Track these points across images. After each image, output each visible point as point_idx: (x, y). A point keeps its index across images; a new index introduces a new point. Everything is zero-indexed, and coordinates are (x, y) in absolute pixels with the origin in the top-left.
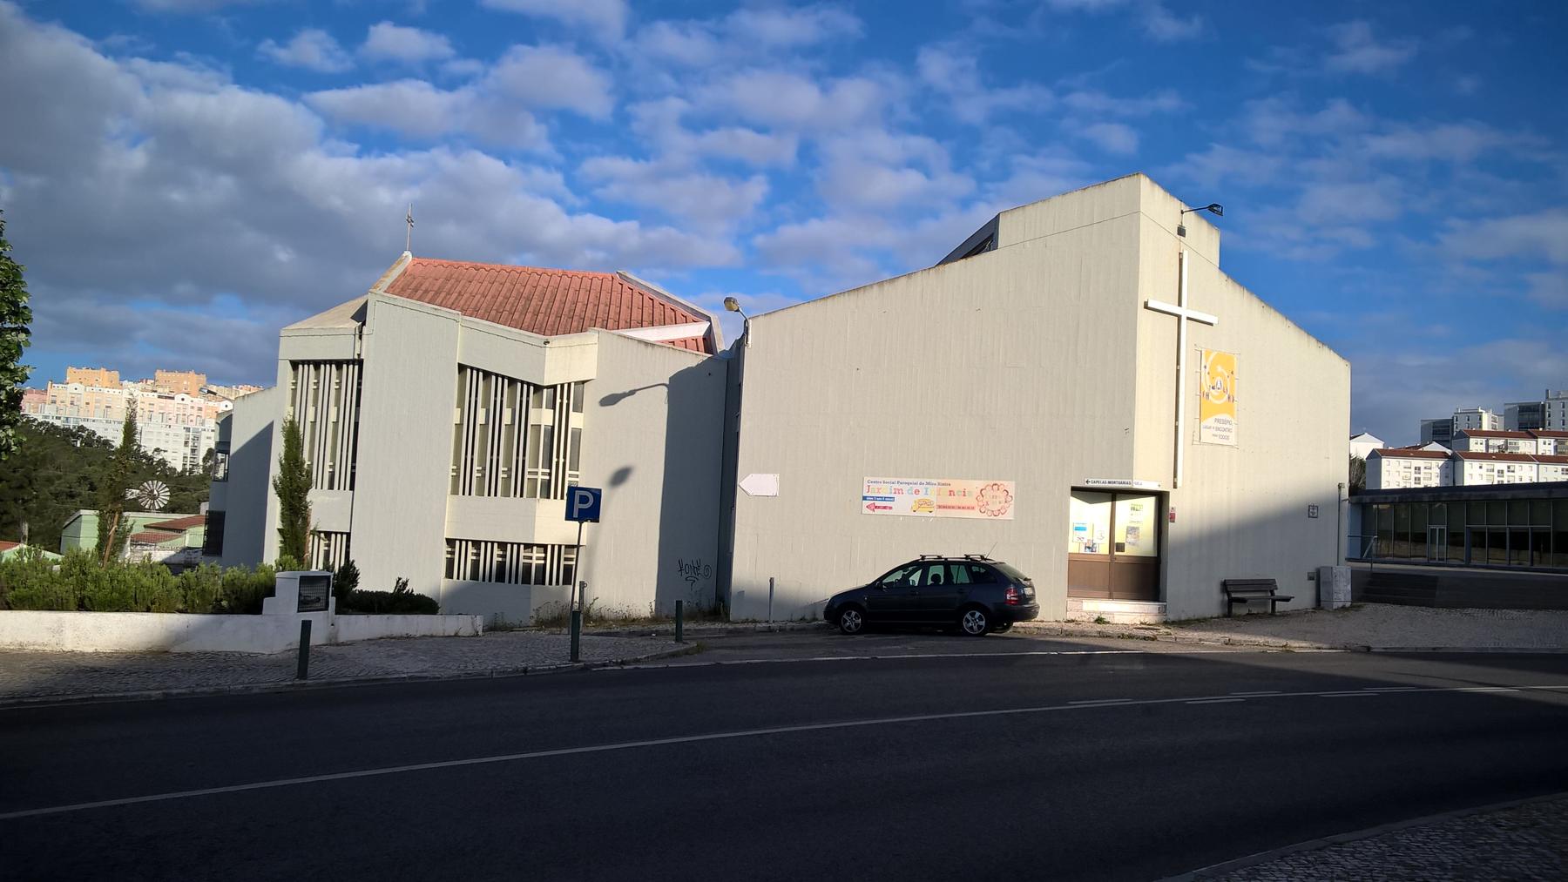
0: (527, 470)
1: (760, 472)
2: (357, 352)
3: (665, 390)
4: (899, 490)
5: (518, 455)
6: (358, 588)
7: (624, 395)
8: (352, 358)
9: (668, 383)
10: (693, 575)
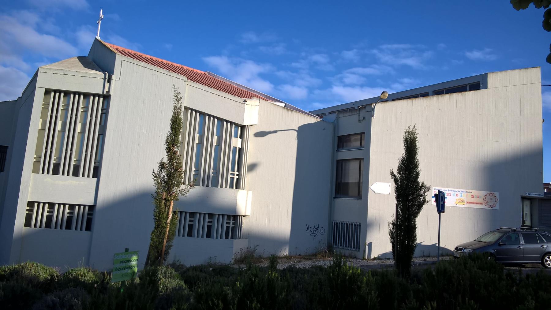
0: (230, 172)
1: (380, 181)
2: (106, 89)
3: (296, 133)
4: (448, 194)
5: (87, 151)
6: (374, 255)
7: (270, 133)
8: (101, 93)
9: (297, 129)
10: (315, 232)
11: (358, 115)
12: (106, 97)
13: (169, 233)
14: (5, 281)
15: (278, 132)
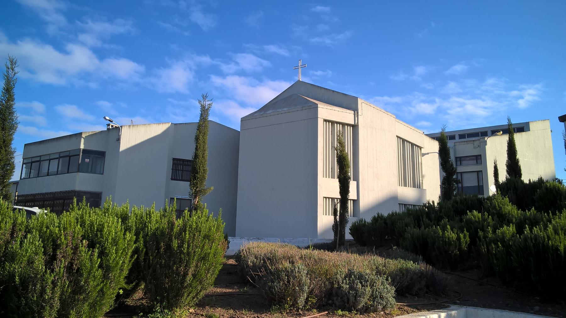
11: (473, 144)
12: (355, 127)
13: (411, 303)
14: (219, 290)
15: (430, 154)
